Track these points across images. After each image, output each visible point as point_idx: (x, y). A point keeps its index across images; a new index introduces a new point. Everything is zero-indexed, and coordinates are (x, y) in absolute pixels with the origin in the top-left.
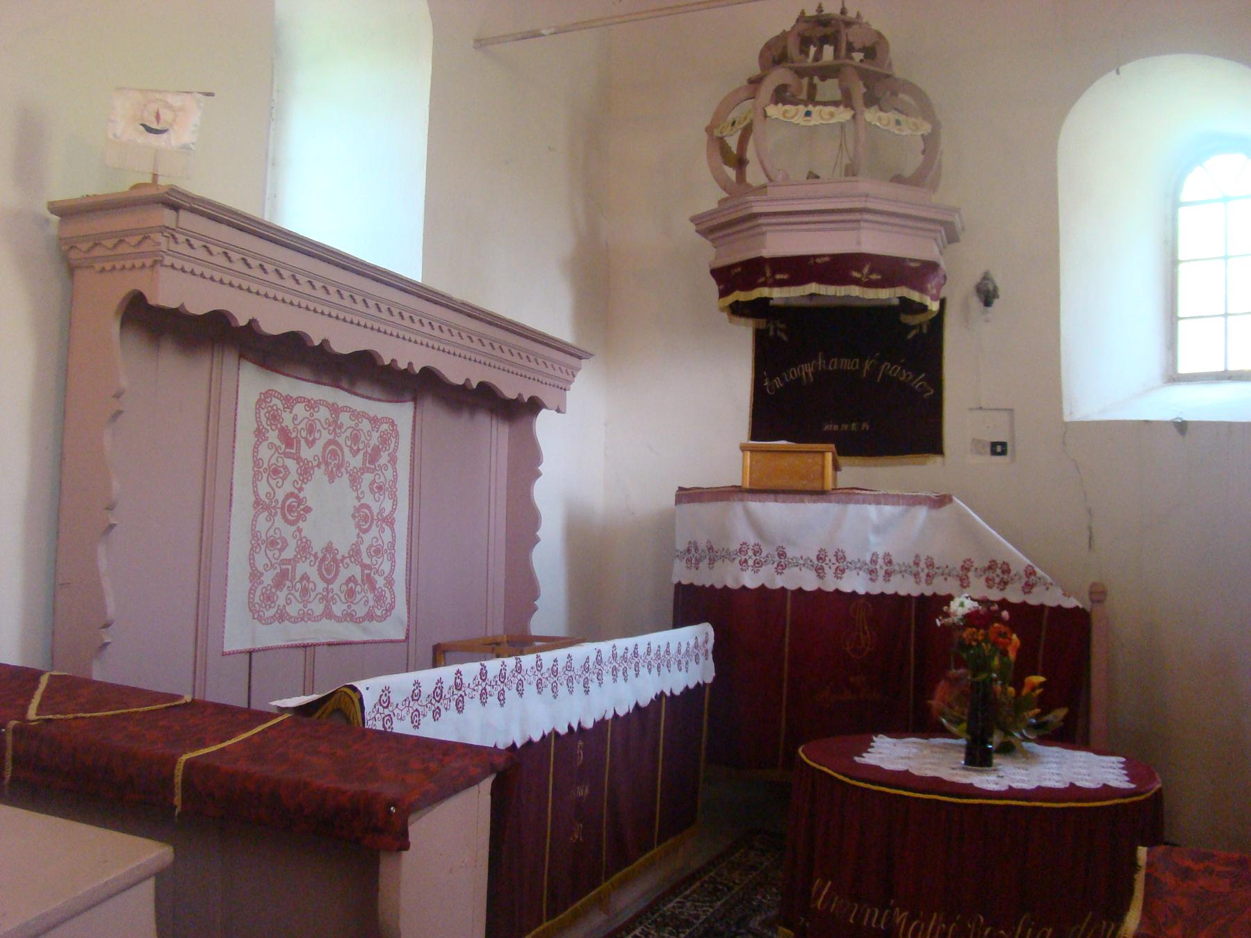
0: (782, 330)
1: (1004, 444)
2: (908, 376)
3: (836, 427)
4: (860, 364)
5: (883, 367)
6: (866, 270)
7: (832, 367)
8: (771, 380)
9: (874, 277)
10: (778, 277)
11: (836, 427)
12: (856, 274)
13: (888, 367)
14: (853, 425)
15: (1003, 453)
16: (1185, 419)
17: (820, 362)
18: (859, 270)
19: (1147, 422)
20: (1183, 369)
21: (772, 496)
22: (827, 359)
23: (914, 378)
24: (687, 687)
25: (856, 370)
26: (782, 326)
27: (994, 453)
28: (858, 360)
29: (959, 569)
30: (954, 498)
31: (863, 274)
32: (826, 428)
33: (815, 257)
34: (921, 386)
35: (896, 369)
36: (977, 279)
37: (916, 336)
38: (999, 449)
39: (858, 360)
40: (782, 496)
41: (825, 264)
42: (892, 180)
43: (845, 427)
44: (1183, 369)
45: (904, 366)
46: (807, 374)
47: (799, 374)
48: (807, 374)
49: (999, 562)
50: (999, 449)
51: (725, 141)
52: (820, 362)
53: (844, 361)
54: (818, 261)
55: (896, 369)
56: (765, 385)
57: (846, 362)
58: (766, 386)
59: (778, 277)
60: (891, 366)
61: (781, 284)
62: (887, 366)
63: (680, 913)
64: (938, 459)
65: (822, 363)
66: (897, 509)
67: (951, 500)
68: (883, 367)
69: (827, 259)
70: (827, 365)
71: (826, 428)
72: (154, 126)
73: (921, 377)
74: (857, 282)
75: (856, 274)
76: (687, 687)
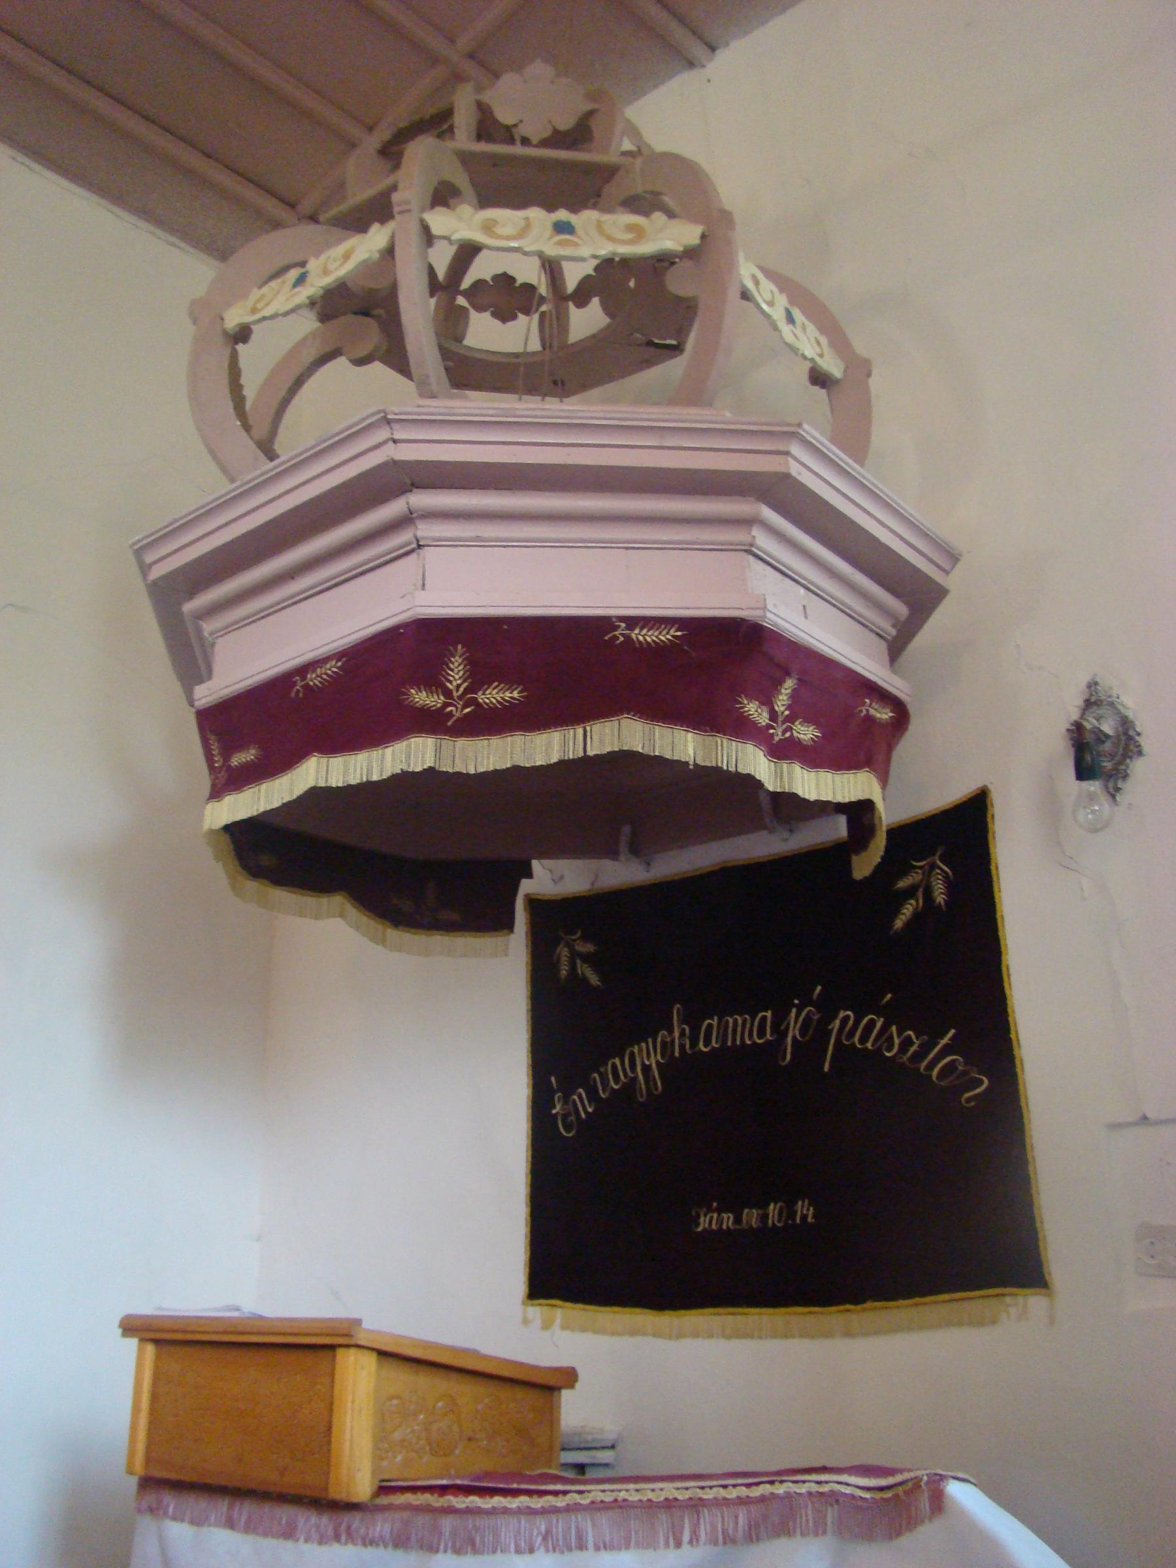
0: (586, 958)
2: (905, 1044)
3: (728, 1220)
4: (775, 1029)
5: (837, 1023)
6: (456, 674)
7: (706, 1046)
8: (566, 1099)
9: (493, 696)
10: (237, 759)
11: (728, 1220)
12: (422, 698)
13: (851, 1022)
14: (772, 1206)
17: (677, 1034)
21: (222, 1505)
22: (693, 1020)
23: (925, 1049)
25: (768, 1042)
26: (588, 948)
28: (769, 1014)
30: (955, 1490)
31: (448, 693)
32: (703, 1223)
33: (303, 670)
34: (950, 1068)
35: (872, 1023)
37: (916, 916)
39: (769, 1014)
40: (245, 1510)
41: (335, 679)
42: (393, 258)
43: (751, 1217)
45: (892, 1015)
46: (646, 1069)
47: (630, 1075)
48: (646, 1069)
52: (677, 1034)
53: (735, 1021)
54: (313, 679)
55: (872, 1023)
56: (554, 1111)
57: (740, 1022)
58: (556, 1115)
59: (237, 759)
60: (753, 1019)
62: (845, 1020)
64: (1035, 1302)
65: (682, 1033)
67: (938, 1501)
68: (837, 1023)
69: (332, 667)
70: (694, 1042)
71: (703, 1223)
73: (945, 1041)
75: (422, 698)
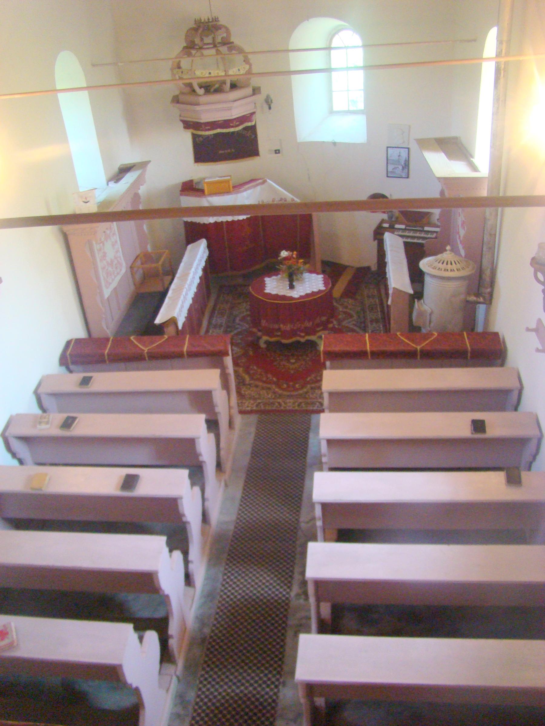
1: (279, 150)
6: (234, 123)
12: (231, 125)
15: (279, 153)
16: (336, 141)
18: (233, 123)
19: (324, 142)
20: (335, 109)
24: (202, 269)
27: (276, 153)
29: (271, 201)
30: (268, 180)
36: (265, 97)
38: (277, 152)
44: (335, 109)
49: (283, 198)
50: (277, 152)
51: (265, 281)
61: (209, 130)
63: (299, 406)
64: (258, 158)
66: (252, 190)
72: (86, 201)
74: (232, 127)
76: (202, 269)
